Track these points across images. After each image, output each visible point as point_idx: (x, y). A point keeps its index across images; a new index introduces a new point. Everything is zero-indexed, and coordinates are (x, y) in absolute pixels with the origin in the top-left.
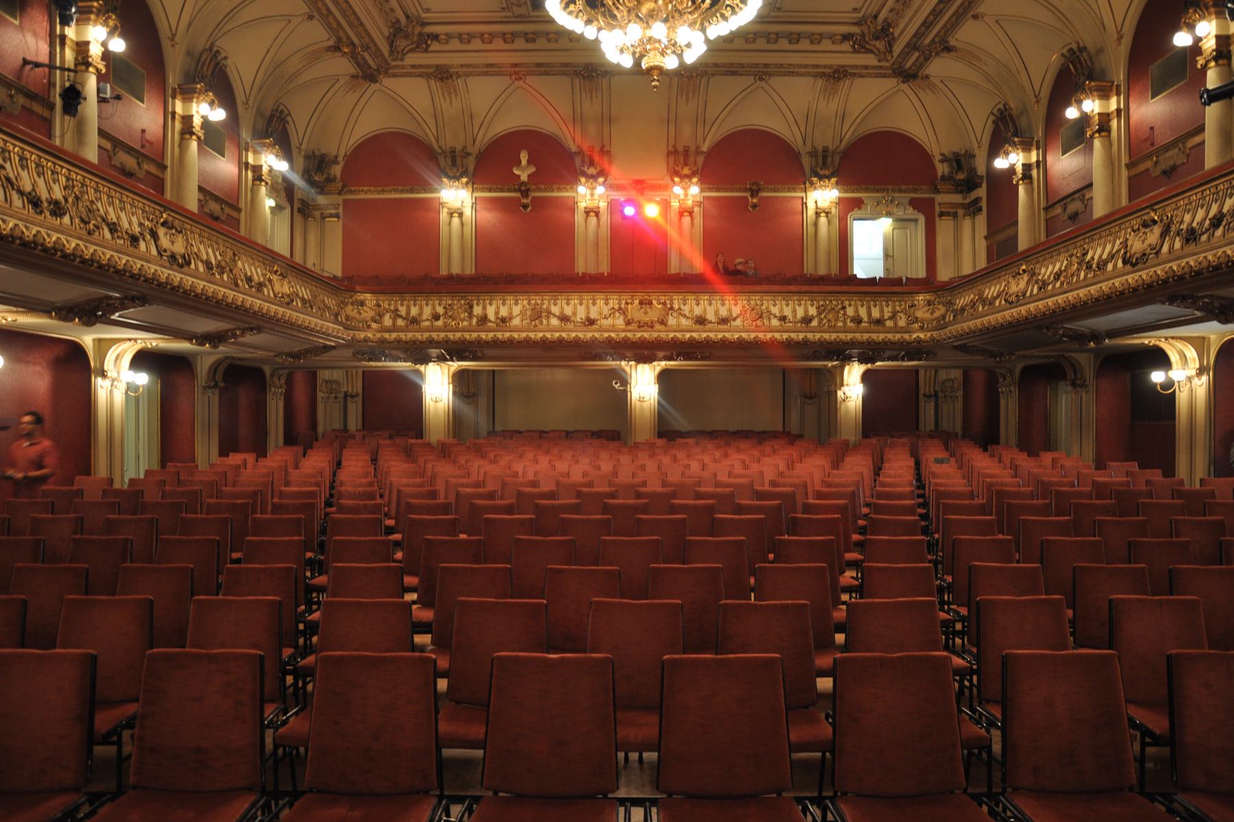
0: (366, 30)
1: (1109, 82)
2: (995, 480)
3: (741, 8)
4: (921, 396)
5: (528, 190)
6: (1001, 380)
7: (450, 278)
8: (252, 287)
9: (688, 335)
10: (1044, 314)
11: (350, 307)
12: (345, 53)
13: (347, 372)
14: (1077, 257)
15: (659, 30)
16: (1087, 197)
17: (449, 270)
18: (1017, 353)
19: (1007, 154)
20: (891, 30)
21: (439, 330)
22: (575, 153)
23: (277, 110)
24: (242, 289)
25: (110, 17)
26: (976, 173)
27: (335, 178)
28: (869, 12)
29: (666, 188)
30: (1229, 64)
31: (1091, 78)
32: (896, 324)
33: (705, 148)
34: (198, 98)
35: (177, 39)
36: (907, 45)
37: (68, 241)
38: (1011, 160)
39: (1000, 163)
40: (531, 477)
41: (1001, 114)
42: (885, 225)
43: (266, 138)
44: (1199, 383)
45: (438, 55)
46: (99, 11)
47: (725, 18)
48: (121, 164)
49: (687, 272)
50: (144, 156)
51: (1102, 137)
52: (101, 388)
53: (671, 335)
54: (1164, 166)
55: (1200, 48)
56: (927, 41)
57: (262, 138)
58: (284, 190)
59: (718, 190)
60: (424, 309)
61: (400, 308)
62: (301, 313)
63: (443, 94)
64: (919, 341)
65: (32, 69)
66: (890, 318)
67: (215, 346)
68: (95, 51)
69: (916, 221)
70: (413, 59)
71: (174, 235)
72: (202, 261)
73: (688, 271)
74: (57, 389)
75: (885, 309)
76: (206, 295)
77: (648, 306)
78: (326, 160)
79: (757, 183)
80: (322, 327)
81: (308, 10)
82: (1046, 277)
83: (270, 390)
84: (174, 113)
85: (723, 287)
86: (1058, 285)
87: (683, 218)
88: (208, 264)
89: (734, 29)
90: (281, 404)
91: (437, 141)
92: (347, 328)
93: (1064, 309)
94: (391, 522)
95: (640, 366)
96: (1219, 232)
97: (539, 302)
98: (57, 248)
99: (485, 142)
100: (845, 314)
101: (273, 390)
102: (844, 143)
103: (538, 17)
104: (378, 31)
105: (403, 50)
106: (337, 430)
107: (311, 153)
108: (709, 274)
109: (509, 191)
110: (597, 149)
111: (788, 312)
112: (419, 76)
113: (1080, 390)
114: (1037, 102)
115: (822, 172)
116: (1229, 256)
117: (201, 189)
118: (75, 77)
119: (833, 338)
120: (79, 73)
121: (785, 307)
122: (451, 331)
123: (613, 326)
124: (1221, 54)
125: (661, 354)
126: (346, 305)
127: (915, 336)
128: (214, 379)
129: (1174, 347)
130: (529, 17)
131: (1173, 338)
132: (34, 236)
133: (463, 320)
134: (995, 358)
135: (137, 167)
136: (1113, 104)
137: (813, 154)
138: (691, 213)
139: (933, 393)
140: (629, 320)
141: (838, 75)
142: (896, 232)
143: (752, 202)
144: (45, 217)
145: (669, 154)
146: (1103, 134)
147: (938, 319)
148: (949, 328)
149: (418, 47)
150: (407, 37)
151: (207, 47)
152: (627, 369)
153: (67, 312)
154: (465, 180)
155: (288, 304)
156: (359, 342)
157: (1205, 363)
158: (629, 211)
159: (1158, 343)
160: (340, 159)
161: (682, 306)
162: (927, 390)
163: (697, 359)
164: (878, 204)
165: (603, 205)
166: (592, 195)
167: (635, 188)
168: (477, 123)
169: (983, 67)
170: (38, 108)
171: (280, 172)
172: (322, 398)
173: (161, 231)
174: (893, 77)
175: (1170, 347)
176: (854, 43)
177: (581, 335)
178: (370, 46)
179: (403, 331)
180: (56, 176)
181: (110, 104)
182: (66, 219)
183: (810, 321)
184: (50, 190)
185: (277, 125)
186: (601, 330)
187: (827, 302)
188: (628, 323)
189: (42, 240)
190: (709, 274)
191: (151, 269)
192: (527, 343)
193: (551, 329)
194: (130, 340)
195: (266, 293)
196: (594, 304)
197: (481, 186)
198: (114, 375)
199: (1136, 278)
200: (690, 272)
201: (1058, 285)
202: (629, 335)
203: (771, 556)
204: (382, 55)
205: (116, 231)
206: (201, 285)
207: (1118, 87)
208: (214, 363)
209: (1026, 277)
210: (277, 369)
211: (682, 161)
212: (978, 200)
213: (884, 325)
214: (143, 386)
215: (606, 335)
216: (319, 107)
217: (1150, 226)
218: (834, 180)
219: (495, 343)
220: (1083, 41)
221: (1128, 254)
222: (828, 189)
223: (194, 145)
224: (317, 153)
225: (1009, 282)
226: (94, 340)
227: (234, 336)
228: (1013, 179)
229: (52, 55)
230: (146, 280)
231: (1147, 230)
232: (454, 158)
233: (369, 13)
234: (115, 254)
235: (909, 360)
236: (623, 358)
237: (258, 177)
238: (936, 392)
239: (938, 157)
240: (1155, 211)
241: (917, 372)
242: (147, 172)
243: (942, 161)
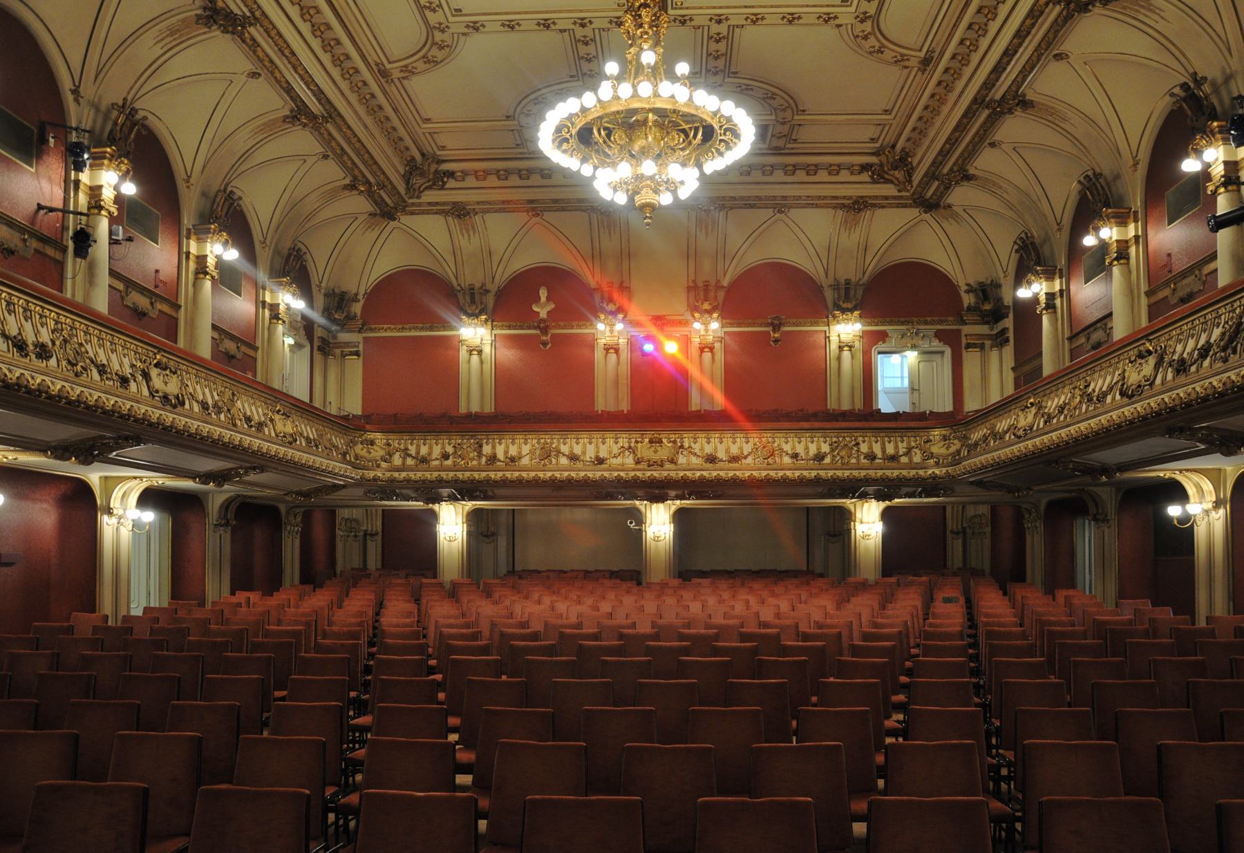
0: (381, 169)
1: (1127, 208)
2: (991, 620)
3: (735, 143)
4: (948, 533)
5: (547, 327)
6: (1027, 516)
7: (469, 416)
8: (251, 426)
9: (698, 474)
10: (1058, 446)
11: (360, 446)
12: (362, 191)
13: (367, 510)
14: (1080, 389)
15: (649, 167)
16: (1109, 326)
17: (468, 409)
18: (1035, 488)
19: (1029, 283)
20: (910, 160)
22: (594, 289)
23: (294, 249)
24: (240, 429)
25: (122, 162)
26: (1002, 303)
27: (355, 316)
28: (887, 140)
29: (686, 323)
30: (1239, 191)
31: (1108, 206)
32: (911, 460)
33: (725, 283)
34: (212, 238)
35: (192, 181)
36: (926, 175)
37: (53, 383)
38: (1034, 289)
39: (1024, 293)
40: (573, 619)
41: (1023, 243)
42: (912, 356)
43: (284, 277)
44: (1217, 516)
45: (453, 192)
46: (112, 156)
47: (721, 154)
48: (134, 303)
49: (707, 408)
50: (158, 296)
51: (1121, 264)
52: (107, 524)
53: (681, 474)
54: (1181, 293)
55: (1209, 174)
56: (946, 170)
57: (279, 277)
58: (306, 328)
59: (739, 325)
60: (433, 448)
61: (410, 447)
62: (304, 452)
63: (461, 230)
64: (934, 477)
65: (46, 213)
66: (904, 454)
67: (220, 485)
68: (108, 195)
69: (942, 353)
70: (430, 196)
71: (167, 375)
72: (197, 401)
73: (708, 407)
74: (64, 526)
75: (900, 445)
76: (200, 435)
77: (658, 445)
78: (347, 298)
80: (333, 468)
81: (322, 150)
82: (1051, 410)
83: (286, 528)
84: (188, 254)
85: (748, 425)
86: (1062, 418)
87: (704, 354)
88: (204, 406)
89: (729, 164)
90: (297, 543)
91: (456, 278)
92: (355, 467)
93: (1067, 443)
94: (433, 662)
95: (654, 506)
96: (1206, 363)
97: (549, 441)
98: (42, 391)
99: (506, 276)
100: (858, 451)
101: (288, 528)
103: (524, 153)
104: (393, 169)
105: (420, 187)
106: (356, 569)
107: (331, 291)
108: (732, 409)
110: (616, 285)
111: (800, 449)
112: (436, 213)
113: (1102, 525)
114: (1059, 230)
115: (845, 305)
116: (1215, 387)
117: (215, 327)
118: (88, 221)
119: (846, 475)
120: (91, 217)
121: (797, 444)
122: (460, 471)
124: (1231, 179)
125: (672, 493)
126: (356, 444)
127: (930, 472)
128: (225, 517)
129: (1190, 480)
131: (1187, 470)
132: (18, 378)
134: (1013, 493)
135: (150, 307)
136: (1131, 230)
137: (836, 286)
138: (712, 349)
139: (961, 530)
140: (638, 459)
141: (858, 206)
142: (922, 365)
143: (774, 337)
144: (30, 360)
145: (689, 289)
146: (1122, 261)
147: (954, 455)
148: (964, 463)
149: (434, 184)
150: (422, 175)
151: (222, 188)
152: (642, 508)
153: (62, 451)
154: (484, 317)
155: (290, 443)
156: (368, 481)
157: (1222, 496)
158: (648, 347)
159: (1173, 476)
160: (360, 297)
161: (693, 445)
162: (955, 527)
163: (709, 498)
164: (902, 337)
165: (622, 341)
166: (612, 331)
167: (655, 324)
168: (496, 259)
169: (1005, 195)
170: (50, 251)
171: (299, 310)
172: (342, 536)
173: (154, 372)
174: (913, 207)
175: (1185, 479)
176: (873, 173)
177: (590, 474)
178: (386, 184)
179: (412, 470)
180: (44, 319)
181: (123, 245)
182: (53, 362)
183: (823, 458)
184: (37, 333)
185: (294, 263)
187: (841, 439)
188: (638, 462)
189: (26, 383)
190: (732, 409)
191: (141, 409)
192: (536, 483)
193: (561, 469)
194: (135, 478)
195: (267, 433)
196: (604, 443)
197: (500, 324)
198: (121, 512)
199: (1132, 410)
200: (710, 409)
201: (1062, 418)
202: (639, 474)
203: (814, 699)
204: (398, 193)
205: (105, 372)
206: (194, 425)
207: (1136, 213)
208: (225, 501)
209: (1033, 410)
210: (292, 508)
211: (702, 297)
212: (1004, 331)
213: (899, 462)
214: (150, 523)
215: (616, 474)
216: (340, 243)
217: (1146, 357)
218: (857, 313)
219: (504, 483)
220: (1099, 166)
221: (1125, 386)
222: (850, 324)
223: (208, 284)
224: (337, 291)
225: (1018, 415)
226: (100, 477)
227: (238, 475)
229: (66, 200)
230: (136, 420)
231: (1143, 361)
232: (472, 295)
233: (383, 152)
234: (102, 395)
235: (927, 497)
236: (636, 497)
237: (275, 316)
238: (964, 528)
239: (964, 288)
240: (1150, 341)
241: (944, 508)
242: (160, 311)
243: (967, 292)
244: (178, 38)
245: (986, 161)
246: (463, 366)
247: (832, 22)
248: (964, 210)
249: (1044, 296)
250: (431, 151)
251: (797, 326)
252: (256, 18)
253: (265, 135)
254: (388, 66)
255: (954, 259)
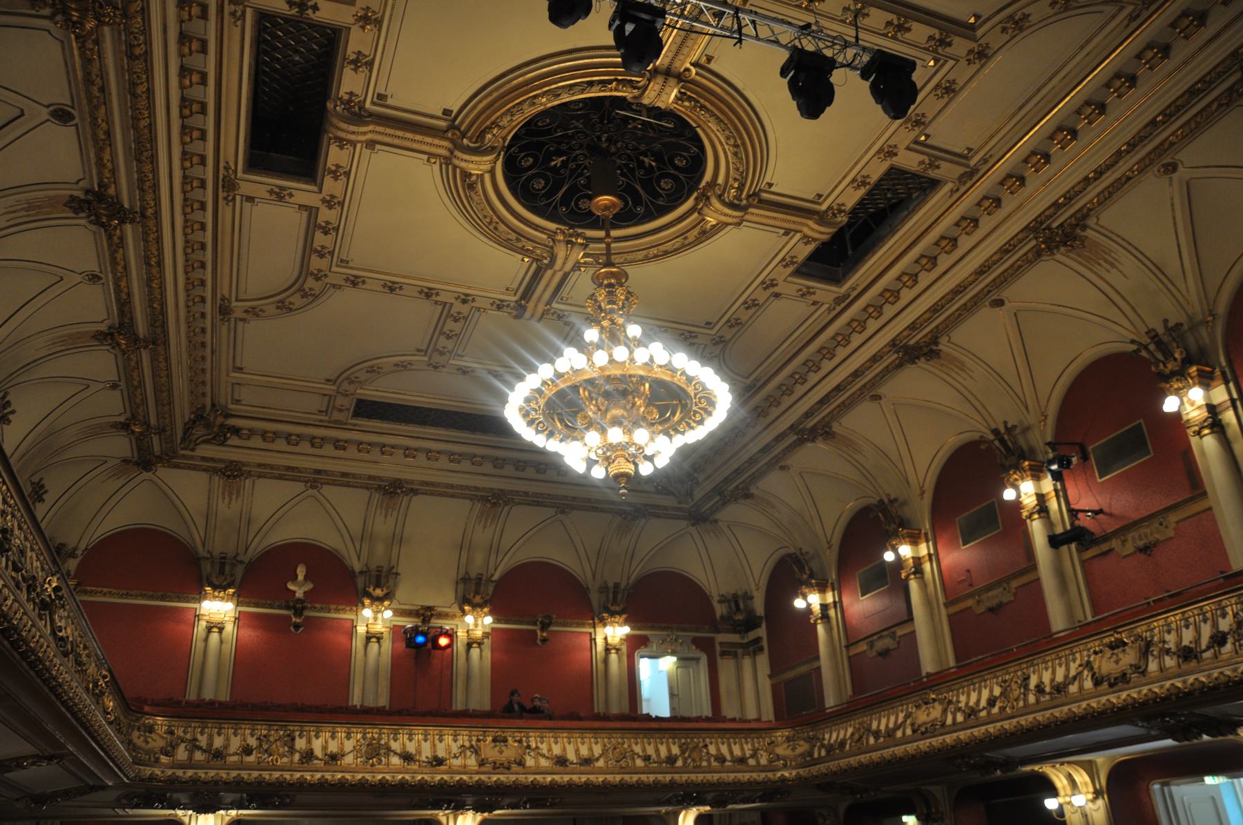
9: (549, 778)
21: (250, 768)
31: (904, 528)
32: (758, 762)
33: (495, 578)
42: (668, 663)
45: (234, 450)
53: (531, 778)
59: (507, 622)
61: (199, 737)
63: (223, 493)
64: (783, 780)
66: (752, 756)
70: (205, 450)
75: (746, 747)
79: (548, 617)
91: (204, 545)
97: (376, 736)
99: (259, 549)
102: (633, 578)
109: (279, 607)
111: (650, 750)
114: (830, 548)
115: (613, 608)
119: (583, 780)
121: (646, 745)
123: (465, 766)
125: (229, 797)
127: (779, 774)
130: (346, 424)
133: (282, 756)
137: (603, 589)
142: (679, 670)
149: (214, 438)
150: (208, 425)
154: (231, 591)
160: (79, 552)
161: (539, 745)
168: (254, 529)
186: (451, 771)
188: (482, 763)
192: (362, 786)
193: (392, 770)
197: (247, 600)
202: (483, 777)
218: (624, 616)
228: (810, 619)
239: (716, 598)
243: (720, 602)
244: (33, 215)
245: (774, 484)
246: (198, 645)
247: (691, 340)
248: (728, 526)
249: (819, 607)
250: (1097, 268)
251: (564, 626)
252: (143, 215)
253: (63, 348)
254: (234, 304)
255: (709, 572)
